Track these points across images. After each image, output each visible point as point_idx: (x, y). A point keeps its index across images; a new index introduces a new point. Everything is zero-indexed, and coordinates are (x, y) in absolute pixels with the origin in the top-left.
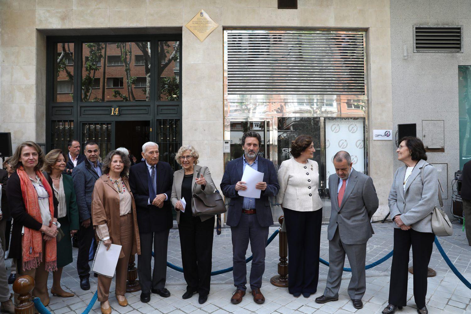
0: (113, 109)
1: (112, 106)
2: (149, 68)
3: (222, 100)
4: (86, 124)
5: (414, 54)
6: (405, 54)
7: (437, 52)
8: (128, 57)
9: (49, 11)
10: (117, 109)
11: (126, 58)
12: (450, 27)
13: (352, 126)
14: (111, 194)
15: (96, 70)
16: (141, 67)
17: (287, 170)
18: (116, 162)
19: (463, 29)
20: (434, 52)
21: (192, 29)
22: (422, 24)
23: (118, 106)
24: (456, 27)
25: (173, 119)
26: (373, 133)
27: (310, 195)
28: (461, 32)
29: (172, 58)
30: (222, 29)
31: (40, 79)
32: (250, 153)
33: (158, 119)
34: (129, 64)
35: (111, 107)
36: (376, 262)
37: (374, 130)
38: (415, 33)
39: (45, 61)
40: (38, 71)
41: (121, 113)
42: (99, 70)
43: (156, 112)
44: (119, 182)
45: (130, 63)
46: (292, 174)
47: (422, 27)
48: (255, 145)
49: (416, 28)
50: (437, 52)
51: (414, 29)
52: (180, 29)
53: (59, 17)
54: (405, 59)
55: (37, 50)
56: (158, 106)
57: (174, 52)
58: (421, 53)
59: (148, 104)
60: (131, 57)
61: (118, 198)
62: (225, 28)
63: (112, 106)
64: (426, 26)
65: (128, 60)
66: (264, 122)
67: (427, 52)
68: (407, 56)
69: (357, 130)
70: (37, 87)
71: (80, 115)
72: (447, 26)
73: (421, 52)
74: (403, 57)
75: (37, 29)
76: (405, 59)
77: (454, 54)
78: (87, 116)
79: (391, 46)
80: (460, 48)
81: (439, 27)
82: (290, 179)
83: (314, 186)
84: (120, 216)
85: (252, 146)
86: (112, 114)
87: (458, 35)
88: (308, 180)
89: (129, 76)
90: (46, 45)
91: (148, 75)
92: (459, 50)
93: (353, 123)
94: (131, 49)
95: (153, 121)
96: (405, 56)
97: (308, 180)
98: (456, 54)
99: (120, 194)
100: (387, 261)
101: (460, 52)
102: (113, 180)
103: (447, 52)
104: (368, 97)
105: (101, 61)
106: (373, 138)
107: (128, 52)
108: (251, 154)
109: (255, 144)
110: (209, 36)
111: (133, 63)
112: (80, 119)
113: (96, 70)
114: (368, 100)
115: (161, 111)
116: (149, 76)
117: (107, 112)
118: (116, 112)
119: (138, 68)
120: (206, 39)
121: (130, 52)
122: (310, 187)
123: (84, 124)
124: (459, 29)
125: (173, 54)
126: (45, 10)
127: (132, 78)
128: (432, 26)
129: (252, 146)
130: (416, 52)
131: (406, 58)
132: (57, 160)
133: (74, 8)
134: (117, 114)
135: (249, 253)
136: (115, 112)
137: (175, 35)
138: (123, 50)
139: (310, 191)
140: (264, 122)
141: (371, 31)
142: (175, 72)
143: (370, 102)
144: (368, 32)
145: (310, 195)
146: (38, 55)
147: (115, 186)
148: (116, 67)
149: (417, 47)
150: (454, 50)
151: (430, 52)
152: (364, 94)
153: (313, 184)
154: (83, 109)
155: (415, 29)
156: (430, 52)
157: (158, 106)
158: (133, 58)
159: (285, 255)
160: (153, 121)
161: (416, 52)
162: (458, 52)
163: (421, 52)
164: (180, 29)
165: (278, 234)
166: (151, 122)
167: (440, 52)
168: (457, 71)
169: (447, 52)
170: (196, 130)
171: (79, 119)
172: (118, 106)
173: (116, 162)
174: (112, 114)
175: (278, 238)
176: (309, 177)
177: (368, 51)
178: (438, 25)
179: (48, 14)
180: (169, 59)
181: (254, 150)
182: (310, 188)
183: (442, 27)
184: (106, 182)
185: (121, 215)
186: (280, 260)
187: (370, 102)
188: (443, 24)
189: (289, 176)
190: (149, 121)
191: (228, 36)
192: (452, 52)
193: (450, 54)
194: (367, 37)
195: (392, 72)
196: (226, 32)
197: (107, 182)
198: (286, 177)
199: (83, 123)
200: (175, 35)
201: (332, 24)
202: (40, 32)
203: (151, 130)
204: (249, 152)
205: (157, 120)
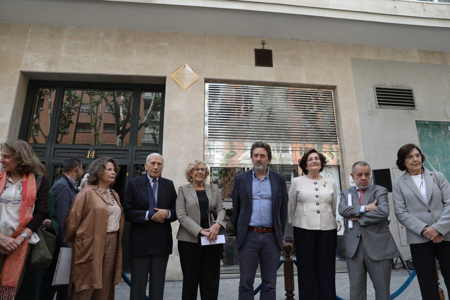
0: (89, 152)
1: (88, 149)
2: (120, 130)
3: (203, 145)
4: (58, 166)
5: (378, 109)
6: (370, 109)
7: (396, 108)
8: (98, 123)
9: (36, 56)
10: (94, 152)
11: (96, 124)
12: (403, 89)
13: (328, 174)
14: (99, 204)
15: (64, 135)
16: (108, 134)
17: (296, 186)
18: (110, 169)
19: (413, 91)
20: (394, 108)
21: (176, 79)
22: (381, 85)
23: (95, 149)
24: (408, 89)
25: (139, 164)
26: (349, 180)
27: (318, 212)
28: (413, 93)
29: (144, 122)
30: (204, 80)
31: (15, 118)
32: (257, 164)
33: (135, 164)
34: (98, 130)
35: (88, 150)
36: (395, 293)
37: (349, 177)
38: (375, 92)
39: (24, 102)
40: (15, 111)
41: (97, 157)
42: (67, 135)
43: (134, 157)
44: (108, 194)
45: (99, 128)
46: (299, 190)
47: (380, 87)
48: (262, 156)
49: (376, 88)
50: (396, 108)
51: (375, 89)
52: (164, 79)
53: (46, 62)
54: (370, 113)
55: (17, 91)
56: (136, 151)
57: (146, 118)
58: (383, 109)
59: (126, 149)
60: (100, 123)
61: (108, 210)
62: (207, 81)
63: (88, 149)
64: (384, 87)
65: (97, 126)
66: (244, 168)
67: (388, 108)
68: (372, 111)
69: (333, 176)
70: (11, 126)
71: (53, 157)
72: (401, 88)
73: (383, 108)
74: (368, 111)
75: (21, 71)
76: (370, 113)
77: (410, 110)
78: (60, 158)
79: (357, 101)
80: (414, 106)
81: (394, 88)
82: (298, 195)
83: (324, 202)
84: (107, 233)
85: (259, 156)
86: (88, 157)
87: (410, 95)
88: (316, 196)
89: (97, 141)
90: (27, 88)
91: (119, 136)
92: (414, 108)
93: (329, 170)
94: (101, 116)
95: (131, 166)
96: (370, 111)
97: (316, 196)
98: (412, 111)
99: (110, 206)
100: (411, 284)
101: (415, 109)
102: (103, 190)
103: (404, 109)
104: (341, 145)
105: (70, 127)
106: (349, 184)
107: (98, 118)
108: (258, 165)
109: (262, 155)
110: (192, 86)
111: (101, 131)
112: (52, 161)
113: (64, 133)
114: (341, 149)
115: (139, 156)
116: (120, 137)
117: (82, 155)
118: (92, 155)
119: (105, 135)
120: (189, 88)
121: (101, 119)
122: (318, 204)
123: (56, 166)
124: (411, 91)
125: (145, 119)
126: (33, 55)
127: (100, 143)
128: (389, 87)
129: (259, 156)
130: (379, 107)
131: (371, 112)
132: (60, 127)
133: (63, 55)
134: (92, 157)
135: (258, 282)
136: (91, 156)
137: (158, 85)
138: (93, 117)
139: (318, 208)
140: (244, 168)
141: (339, 89)
142: (142, 143)
143: (343, 150)
144: (335, 90)
145: (318, 212)
146: (18, 95)
147: (105, 196)
148: (84, 133)
149: (379, 104)
150: (409, 108)
151: (390, 108)
152: (337, 144)
153: (322, 201)
154: (57, 151)
155: (375, 89)
156: (390, 108)
157: (136, 151)
158: (102, 125)
159: (292, 289)
160: (131, 166)
161: (379, 107)
162: (413, 109)
163: (383, 108)
164: (164, 79)
165: (283, 265)
166: (128, 166)
167: (398, 108)
168: (415, 126)
169: (404, 109)
170: (175, 174)
171: (51, 160)
172: (95, 149)
173: (110, 169)
174: (88, 157)
175: (283, 266)
176: (317, 193)
177: (337, 106)
178: (394, 86)
179: (35, 59)
180: (141, 123)
181: (261, 161)
182: (318, 204)
183: (397, 88)
184: (95, 191)
185: (108, 231)
186: (286, 295)
187: (344, 150)
188: (397, 86)
189: (297, 191)
190: (127, 165)
191: (209, 87)
192: (409, 109)
193: (407, 111)
194: (335, 94)
195: (360, 125)
196: (207, 85)
197: (96, 191)
198: (295, 193)
199: (55, 166)
200: (158, 85)
201: (304, 81)
202: (24, 74)
203: (127, 174)
204: (256, 163)
205: (135, 164)
